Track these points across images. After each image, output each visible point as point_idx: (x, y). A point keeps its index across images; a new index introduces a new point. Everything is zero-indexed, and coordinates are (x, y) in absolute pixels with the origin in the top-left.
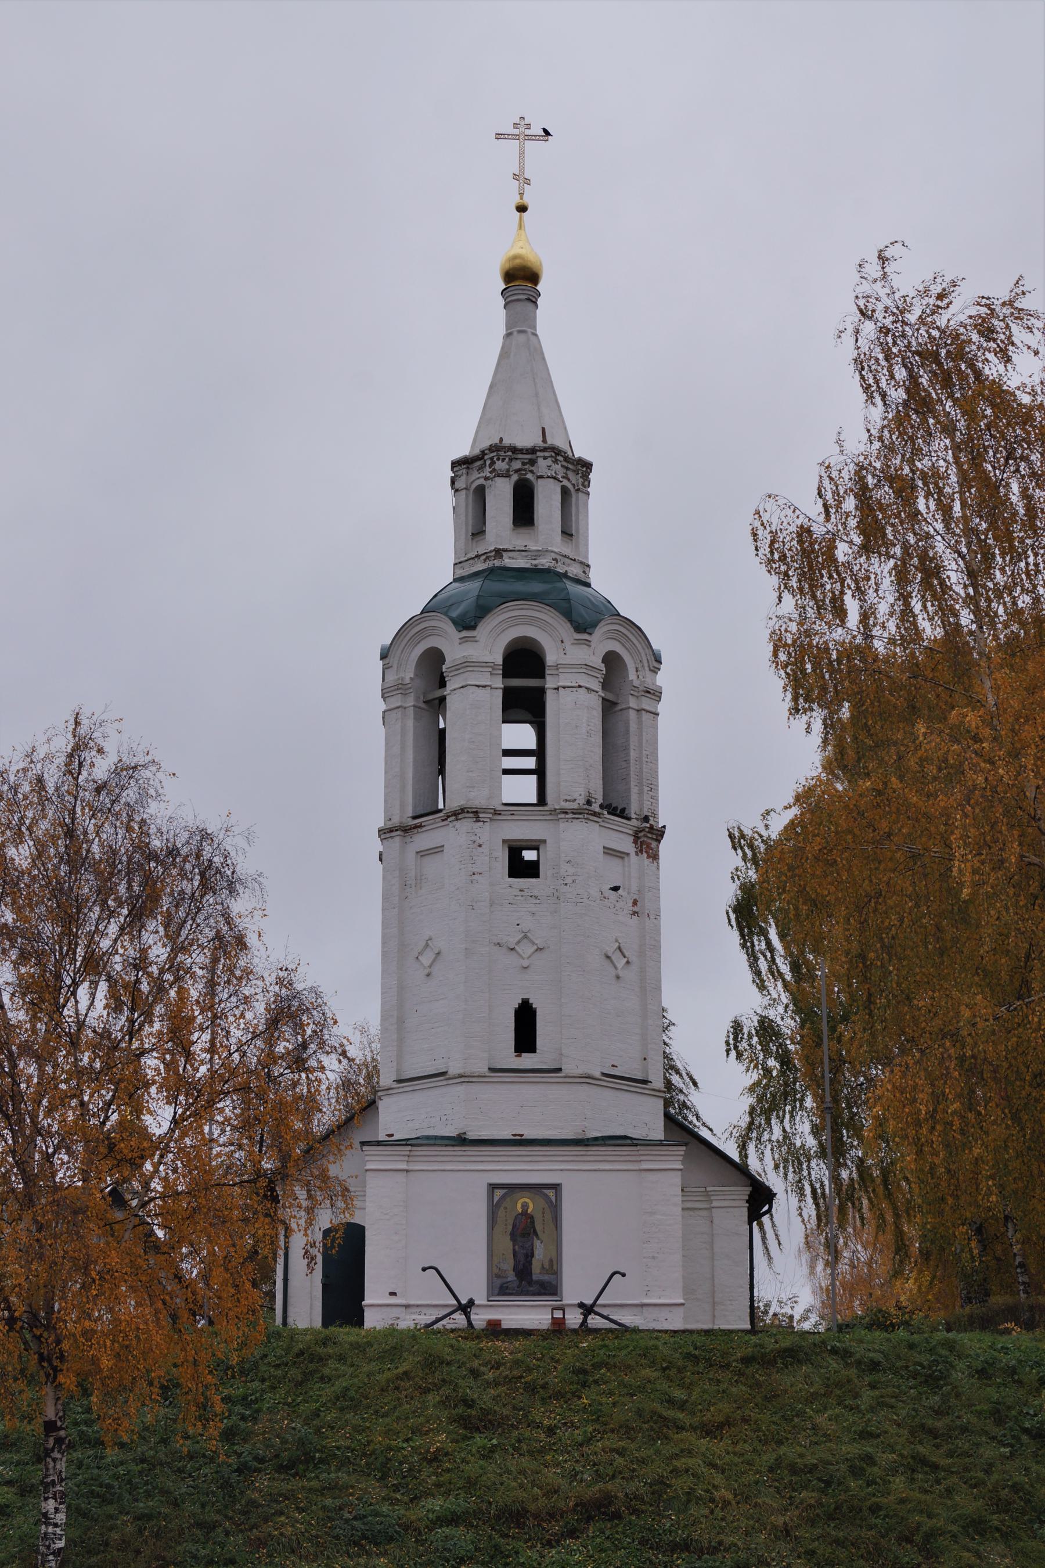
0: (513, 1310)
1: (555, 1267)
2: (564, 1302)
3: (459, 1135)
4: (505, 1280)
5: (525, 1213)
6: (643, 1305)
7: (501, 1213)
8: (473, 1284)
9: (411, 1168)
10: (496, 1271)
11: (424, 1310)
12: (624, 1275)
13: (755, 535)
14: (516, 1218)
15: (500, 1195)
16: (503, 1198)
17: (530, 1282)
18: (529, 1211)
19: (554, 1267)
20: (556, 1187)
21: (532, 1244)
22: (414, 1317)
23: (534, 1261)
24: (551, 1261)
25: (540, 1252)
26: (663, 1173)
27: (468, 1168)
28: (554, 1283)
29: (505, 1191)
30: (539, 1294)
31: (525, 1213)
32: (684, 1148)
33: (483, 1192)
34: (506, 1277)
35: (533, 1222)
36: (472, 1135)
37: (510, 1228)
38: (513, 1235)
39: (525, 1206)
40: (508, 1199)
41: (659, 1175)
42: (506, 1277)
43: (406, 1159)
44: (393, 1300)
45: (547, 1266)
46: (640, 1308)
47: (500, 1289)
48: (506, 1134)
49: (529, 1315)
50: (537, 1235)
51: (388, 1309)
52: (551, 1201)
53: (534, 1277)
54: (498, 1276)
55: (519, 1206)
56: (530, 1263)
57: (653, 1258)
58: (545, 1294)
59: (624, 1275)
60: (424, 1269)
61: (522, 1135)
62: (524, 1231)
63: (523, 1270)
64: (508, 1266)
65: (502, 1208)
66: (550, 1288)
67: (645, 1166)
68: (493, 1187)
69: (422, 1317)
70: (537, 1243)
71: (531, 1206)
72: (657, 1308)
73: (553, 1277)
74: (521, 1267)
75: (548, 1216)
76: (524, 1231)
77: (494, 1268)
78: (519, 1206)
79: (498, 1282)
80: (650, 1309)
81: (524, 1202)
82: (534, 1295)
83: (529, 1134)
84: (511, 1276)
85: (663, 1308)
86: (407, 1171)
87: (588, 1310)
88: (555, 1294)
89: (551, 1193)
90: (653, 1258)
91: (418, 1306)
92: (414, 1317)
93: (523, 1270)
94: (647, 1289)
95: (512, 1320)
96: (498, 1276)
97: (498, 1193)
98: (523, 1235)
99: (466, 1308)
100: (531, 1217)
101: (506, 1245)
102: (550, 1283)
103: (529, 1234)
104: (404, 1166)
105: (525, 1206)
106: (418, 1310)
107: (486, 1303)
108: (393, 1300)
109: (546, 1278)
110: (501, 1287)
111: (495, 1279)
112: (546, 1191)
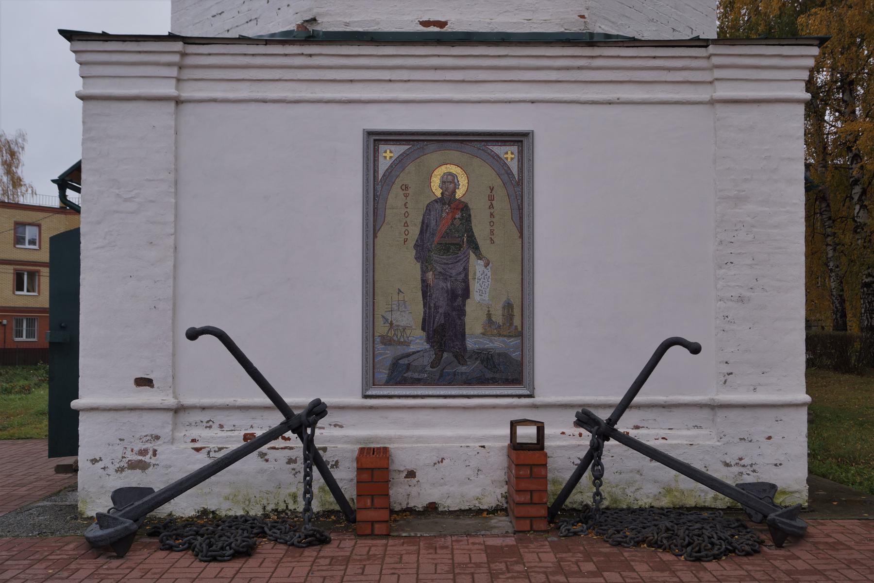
0: (423, 415)
1: (517, 321)
2: (538, 399)
3: (302, 26)
4: (401, 350)
5: (448, 199)
6: (714, 407)
7: (394, 199)
8: (323, 359)
9: (185, 94)
10: (382, 329)
11: (219, 417)
12: (695, 349)
13: (491, 198)
14: (429, 208)
15: (391, 153)
16: (399, 163)
17: (461, 355)
18: (459, 194)
19: (516, 320)
20: (520, 140)
21: (466, 270)
22: (195, 433)
23: (470, 307)
24: (508, 306)
25: (484, 289)
26: (765, 107)
27: (329, 95)
28: (516, 355)
29: (403, 148)
30: (482, 381)
31: (448, 199)
32: (815, 51)
33: (356, 149)
34: (407, 344)
35: (467, 219)
36: (328, 24)
37: (415, 232)
38: (422, 252)
39: (449, 182)
40: (411, 168)
41: (754, 114)
42: (407, 344)
43: (174, 72)
44: (144, 397)
45: (498, 317)
46: (705, 413)
47: (391, 371)
48: (409, 23)
49: (451, 445)
50: (476, 248)
51: (133, 417)
52: (509, 172)
53: (470, 344)
54: (387, 341)
55: (436, 182)
56: (462, 312)
57: (741, 299)
58: (494, 382)
59: (695, 349)
60: (193, 335)
61: (442, 24)
62: (447, 238)
63: (445, 328)
64: (410, 317)
65: (396, 189)
66: (505, 370)
67: (723, 91)
68: (376, 139)
69: (215, 432)
70: (477, 266)
71: (463, 181)
72: (748, 414)
73: (513, 342)
74: (440, 319)
75: (502, 204)
76: (447, 238)
77: (379, 322)
78: (436, 182)
79: (388, 354)
80: (733, 414)
81: (444, 172)
82: (468, 382)
83: (460, 20)
84: (418, 341)
85: (760, 412)
86: (178, 102)
87: (600, 428)
88: (517, 381)
89: (509, 154)
90: (741, 299)
91: (203, 408)
92: (195, 433)
93: (445, 328)
94: (727, 369)
95: (419, 439)
96: (387, 341)
97: (389, 154)
98: (445, 248)
99: (304, 421)
100: (464, 208)
101: (405, 270)
102: (504, 356)
103: (459, 246)
104: (168, 89)
105: (449, 182)
106: (205, 416)
107: (358, 400)
108: (144, 397)
109: (497, 344)
110: (395, 365)
111: (380, 347)
112: (498, 150)
